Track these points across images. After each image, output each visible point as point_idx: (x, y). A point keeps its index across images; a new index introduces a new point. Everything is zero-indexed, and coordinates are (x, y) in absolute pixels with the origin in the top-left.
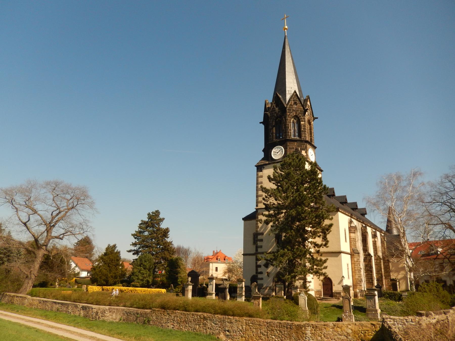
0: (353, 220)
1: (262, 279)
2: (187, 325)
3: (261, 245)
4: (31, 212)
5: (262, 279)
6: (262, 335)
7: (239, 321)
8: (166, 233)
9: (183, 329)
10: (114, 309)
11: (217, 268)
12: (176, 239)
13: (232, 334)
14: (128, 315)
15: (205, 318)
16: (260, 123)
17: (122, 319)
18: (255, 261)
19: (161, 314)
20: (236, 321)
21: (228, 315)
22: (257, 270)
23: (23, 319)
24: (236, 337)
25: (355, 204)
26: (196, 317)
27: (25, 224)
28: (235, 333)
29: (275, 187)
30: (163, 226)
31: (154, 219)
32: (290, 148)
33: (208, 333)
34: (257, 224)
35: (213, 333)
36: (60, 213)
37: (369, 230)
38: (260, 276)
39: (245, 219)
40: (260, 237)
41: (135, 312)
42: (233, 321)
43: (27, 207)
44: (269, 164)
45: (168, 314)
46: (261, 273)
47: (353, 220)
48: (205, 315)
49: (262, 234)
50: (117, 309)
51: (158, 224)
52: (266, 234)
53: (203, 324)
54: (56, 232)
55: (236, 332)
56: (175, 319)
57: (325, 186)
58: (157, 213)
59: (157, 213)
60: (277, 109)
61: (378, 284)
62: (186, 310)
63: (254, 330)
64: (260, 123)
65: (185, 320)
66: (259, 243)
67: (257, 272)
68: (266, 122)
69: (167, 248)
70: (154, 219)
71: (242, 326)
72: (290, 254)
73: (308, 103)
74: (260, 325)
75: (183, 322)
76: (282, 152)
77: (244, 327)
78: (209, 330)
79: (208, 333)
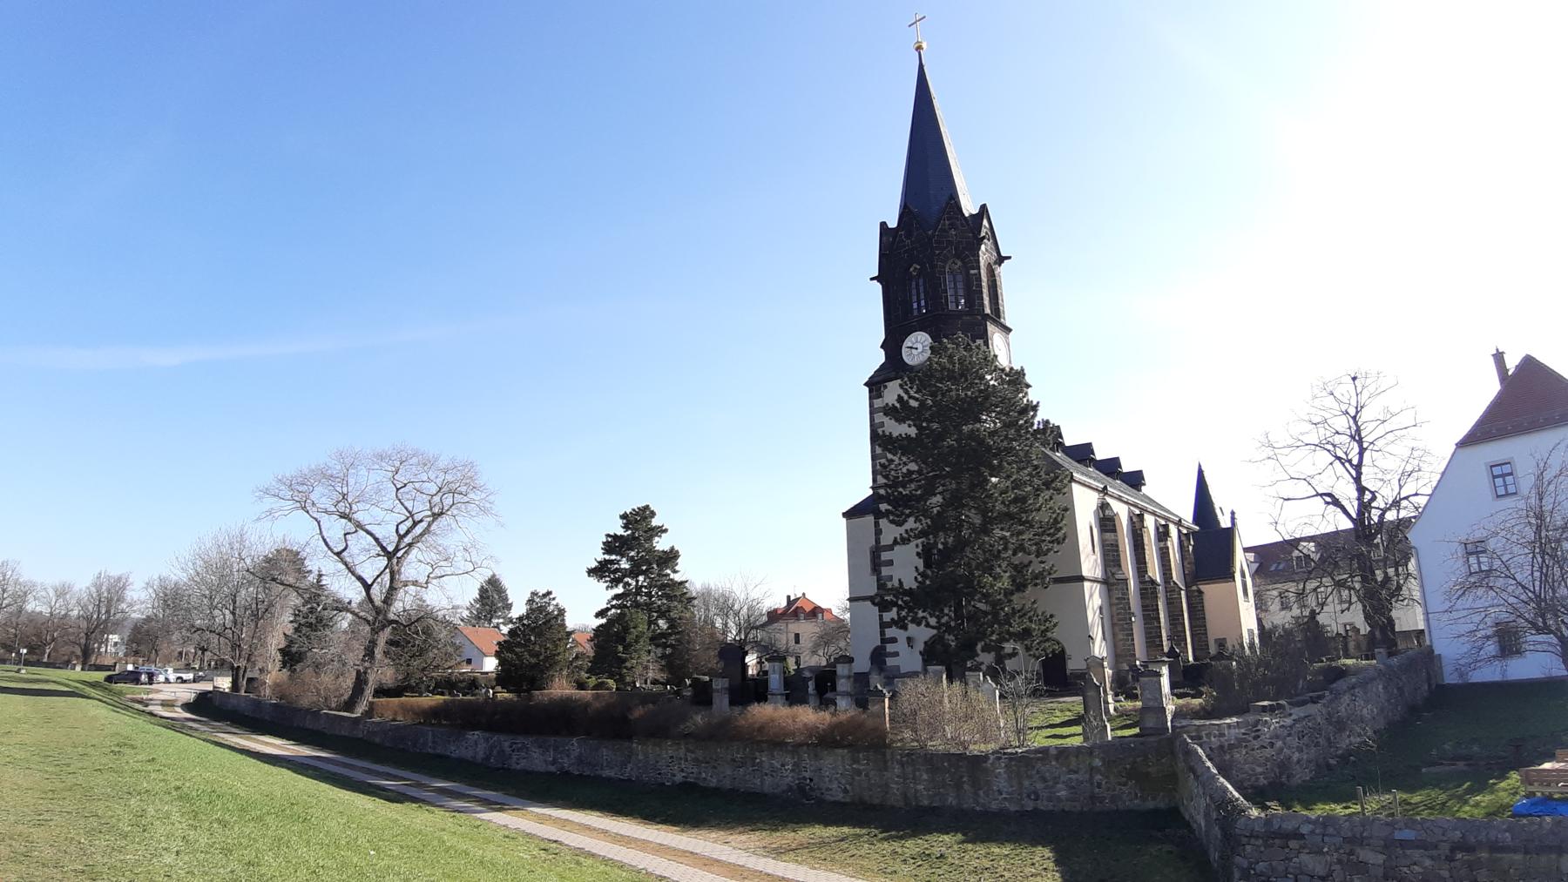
0: (1109, 500)
1: (896, 654)
4: (350, 527)
5: (896, 654)
8: (671, 557)
11: (797, 636)
12: (693, 572)
22: (882, 633)
23: (643, 845)
25: (1115, 462)
27: (338, 554)
29: (913, 432)
30: (661, 544)
31: (640, 523)
36: (415, 524)
37: (1149, 521)
38: (890, 648)
39: (849, 515)
40: (885, 556)
43: (343, 516)
46: (894, 640)
47: (1109, 500)
51: (650, 539)
54: (413, 567)
58: (645, 513)
59: (645, 513)
61: (1172, 648)
66: (885, 571)
67: (884, 641)
68: (886, 276)
69: (676, 593)
70: (640, 523)
72: (175, 817)
73: (985, 222)
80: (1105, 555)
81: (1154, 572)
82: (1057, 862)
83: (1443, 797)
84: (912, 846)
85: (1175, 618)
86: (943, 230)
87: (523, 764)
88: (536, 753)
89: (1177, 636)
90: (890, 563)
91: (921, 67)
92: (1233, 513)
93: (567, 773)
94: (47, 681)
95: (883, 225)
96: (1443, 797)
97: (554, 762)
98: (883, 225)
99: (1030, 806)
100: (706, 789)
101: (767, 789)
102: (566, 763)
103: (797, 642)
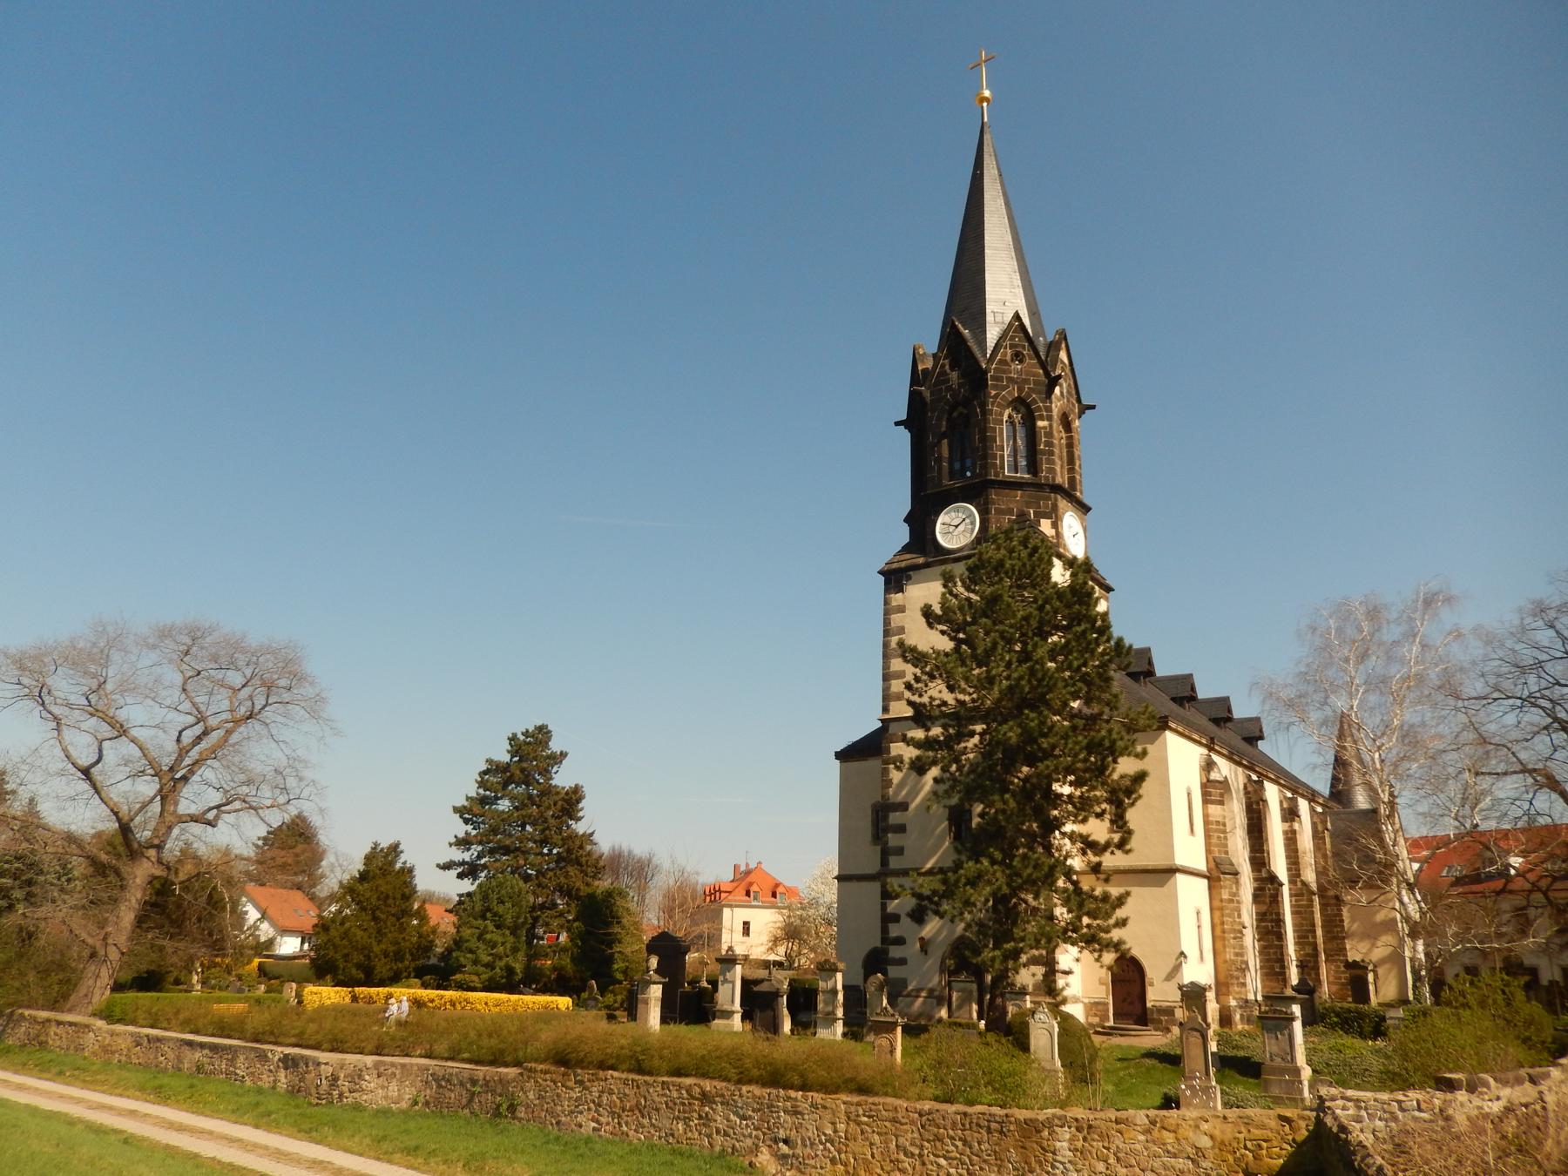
0: (1215, 757)
1: (902, 962)
2: (646, 1121)
3: (900, 843)
4: (105, 730)
5: (902, 962)
6: (902, 1156)
7: (825, 1107)
8: (571, 802)
9: (631, 1133)
10: (393, 1065)
11: (746, 925)
12: (606, 825)
13: (799, 1151)
14: (440, 1086)
15: (705, 1098)
16: (897, 424)
17: (421, 1099)
18: (878, 900)
19: (555, 1083)
20: (814, 1106)
21: (785, 1088)
22: (885, 930)
24: (812, 1162)
25: (1224, 703)
26: (675, 1094)
27: (86, 772)
28: (808, 1150)
29: (946, 644)
30: (563, 778)
31: (530, 756)
32: (999, 512)
33: (717, 1149)
34: (885, 772)
35: (733, 1147)
36: (205, 733)
37: (1272, 793)
38: (895, 952)
39: (844, 755)
40: (895, 818)
41: (466, 1075)
42: (804, 1106)
43: (94, 713)
44: (927, 565)
45: (581, 1083)
46: (900, 941)
47: (1215, 757)
48: (708, 1085)
49: (904, 806)
50: (403, 1066)
51: (546, 772)
52: (917, 807)
53: (700, 1117)
54: (192, 799)
55: (812, 1144)
56: (604, 1099)
57: (1120, 641)
58: (541, 735)
59: (541, 735)
60: (954, 375)
61: (1302, 981)
62: (640, 1070)
63: (876, 1137)
64: (897, 424)
65: (638, 1105)
66: (893, 840)
67: (886, 940)
68: (916, 420)
69: (576, 854)
70: (530, 756)
71: (833, 1124)
72: (999, 874)
73: (1063, 355)
74: (894, 1120)
75: (631, 1110)
76: (973, 523)
77: (841, 1127)
78: (719, 1139)
79: (717, 1149)
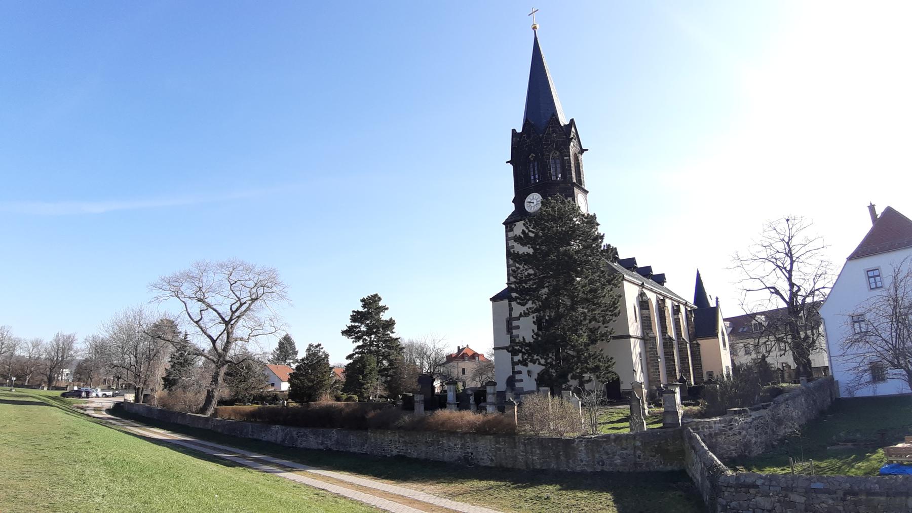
0: (645, 291)
1: (521, 381)
4: (204, 306)
5: (521, 381)
8: (390, 324)
11: (464, 370)
12: (403, 333)
22: (513, 368)
25: (648, 269)
27: (197, 322)
29: (531, 251)
30: (385, 316)
31: (372, 304)
36: (241, 305)
37: (669, 303)
38: (518, 377)
39: (494, 299)
40: (515, 323)
43: (200, 300)
46: (520, 372)
47: (645, 291)
51: (378, 313)
54: (240, 330)
58: (375, 299)
59: (375, 299)
61: (681, 377)
66: (515, 332)
67: (514, 373)
68: (515, 160)
69: (393, 345)
70: (372, 304)
72: (102, 475)
73: (573, 129)
80: (643, 323)
81: (671, 332)
82: (615, 501)
83: (839, 464)
84: (531, 492)
85: (684, 360)
86: (548, 134)
87: (304, 445)
88: (312, 438)
89: (685, 370)
90: (518, 327)
91: (536, 39)
92: (717, 299)
93: (330, 449)
94: (27, 396)
95: (514, 131)
96: (839, 464)
97: (322, 443)
98: (514, 131)
99: (599, 469)
100: (410, 459)
101: (446, 459)
102: (329, 444)
103: (464, 373)
